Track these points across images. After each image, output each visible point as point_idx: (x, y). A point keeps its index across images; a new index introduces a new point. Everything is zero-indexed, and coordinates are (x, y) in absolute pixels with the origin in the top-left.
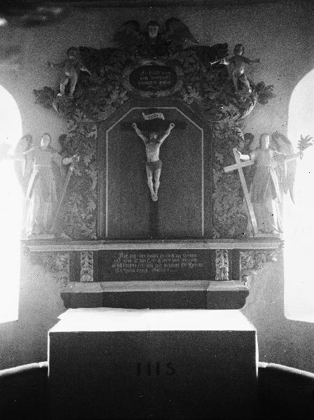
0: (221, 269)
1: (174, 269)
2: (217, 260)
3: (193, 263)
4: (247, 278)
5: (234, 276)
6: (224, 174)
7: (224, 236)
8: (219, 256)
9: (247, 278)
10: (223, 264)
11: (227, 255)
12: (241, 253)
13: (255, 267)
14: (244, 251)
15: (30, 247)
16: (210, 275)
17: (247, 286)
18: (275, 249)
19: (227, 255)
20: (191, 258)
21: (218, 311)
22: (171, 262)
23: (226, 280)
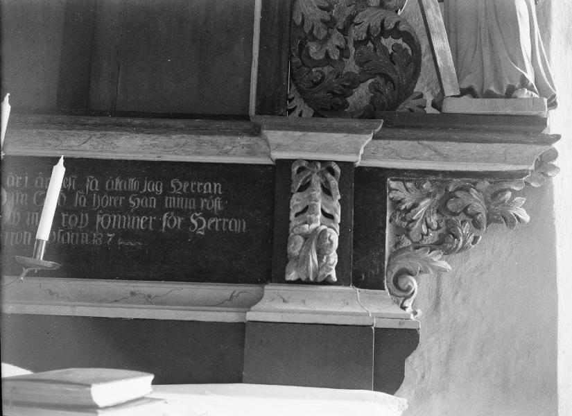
0: (307, 237)
1: (127, 234)
2: (297, 202)
3: (208, 214)
4: (414, 283)
5: (362, 269)
6: (450, 193)
7: (330, 108)
8: (305, 187)
9: (414, 283)
10: (320, 220)
11: (334, 182)
12: (393, 184)
13: (445, 242)
14: (399, 174)
15: (242, 13)
16: (265, 260)
17: (414, 313)
18: (522, 174)
19: (334, 182)
20: (199, 196)
21: (293, 387)
22: (126, 209)
23: (327, 282)
